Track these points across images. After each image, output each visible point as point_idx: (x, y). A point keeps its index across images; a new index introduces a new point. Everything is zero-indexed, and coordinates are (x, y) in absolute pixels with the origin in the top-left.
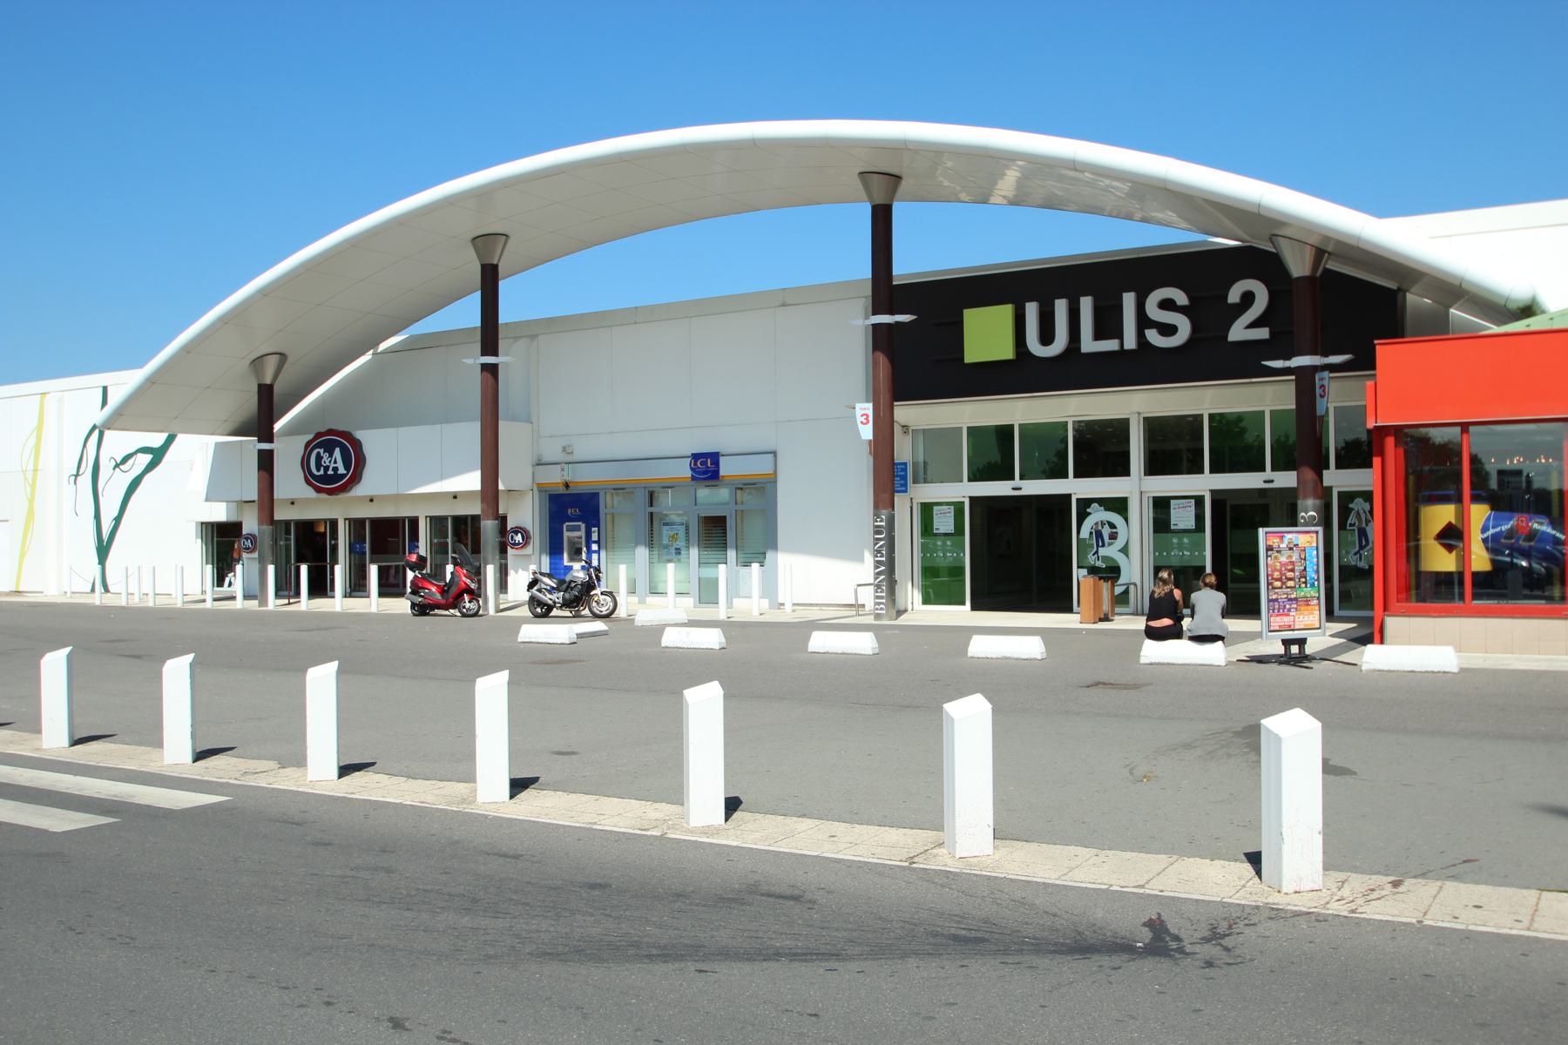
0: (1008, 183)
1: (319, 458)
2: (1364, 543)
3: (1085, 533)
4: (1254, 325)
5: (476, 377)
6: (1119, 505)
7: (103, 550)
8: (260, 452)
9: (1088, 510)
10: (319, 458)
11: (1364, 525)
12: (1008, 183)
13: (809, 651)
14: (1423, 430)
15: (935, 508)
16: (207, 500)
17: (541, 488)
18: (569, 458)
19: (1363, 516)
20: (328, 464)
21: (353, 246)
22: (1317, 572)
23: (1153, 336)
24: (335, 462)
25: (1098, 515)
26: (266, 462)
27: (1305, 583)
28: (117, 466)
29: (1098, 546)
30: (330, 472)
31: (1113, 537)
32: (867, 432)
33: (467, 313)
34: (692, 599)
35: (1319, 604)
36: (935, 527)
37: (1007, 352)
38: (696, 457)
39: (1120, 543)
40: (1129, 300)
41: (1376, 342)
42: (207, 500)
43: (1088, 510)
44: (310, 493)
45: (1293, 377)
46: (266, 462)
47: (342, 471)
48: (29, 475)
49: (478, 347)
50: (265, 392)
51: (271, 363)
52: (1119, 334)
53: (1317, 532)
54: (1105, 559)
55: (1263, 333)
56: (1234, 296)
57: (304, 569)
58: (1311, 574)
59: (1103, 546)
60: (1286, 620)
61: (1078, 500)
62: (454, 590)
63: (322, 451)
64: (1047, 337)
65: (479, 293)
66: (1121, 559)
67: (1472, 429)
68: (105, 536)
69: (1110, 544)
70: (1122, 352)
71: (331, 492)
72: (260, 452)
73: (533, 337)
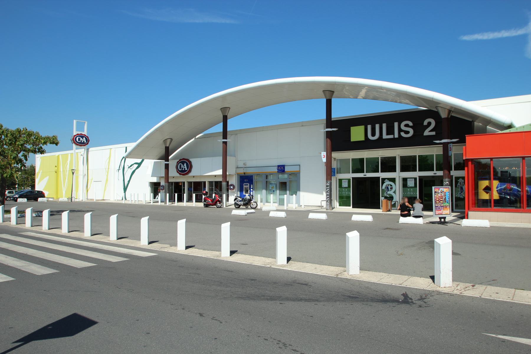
0: (363, 92)
1: (180, 166)
2: (462, 191)
3: (384, 187)
4: (431, 131)
5: (221, 144)
6: (393, 180)
7: (125, 189)
8: (165, 164)
9: (385, 181)
10: (180, 166)
11: (462, 186)
12: (363, 92)
13: (309, 218)
14: (479, 160)
15: (343, 180)
16: (152, 176)
17: (238, 174)
18: (245, 166)
19: (462, 184)
20: (82, 140)
21: (190, 111)
22: (449, 199)
23: (403, 134)
24: (185, 167)
25: (387, 183)
26: (167, 166)
27: (446, 202)
28: (129, 167)
29: (387, 191)
30: (183, 169)
31: (391, 188)
32: (324, 160)
33: (219, 128)
34: (277, 204)
35: (450, 208)
36: (343, 185)
37: (362, 138)
38: (279, 166)
39: (393, 190)
40: (396, 124)
41: (466, 135)
42: (152, 176)
43: (385, 181)
44: (178, 175)
45: (442, 145)
46: (167, 166)
47: (186, 169)
48: (107, 170)
49: (222, 137)
50: (167, 149)
51: (169, 141)
52: (393, 133)
53: (449, 188)
54: (389, 194)
55: (433, 133)
56: (425, 123)
57: (176, 195)
58: (447, 199)
59: (389, 191)
60: (440, 212)
61: (455, 177)
62: (215, 201)
63: (181, 164)
64: (373, 134)
65: (222, 123)
66: (393, 195)
67: (493, 159)
68: (126, 186)
69: (390, 191)
70: (394, 139)
71: (183, 175)
72: (165, 164)
73: (236, 134)
